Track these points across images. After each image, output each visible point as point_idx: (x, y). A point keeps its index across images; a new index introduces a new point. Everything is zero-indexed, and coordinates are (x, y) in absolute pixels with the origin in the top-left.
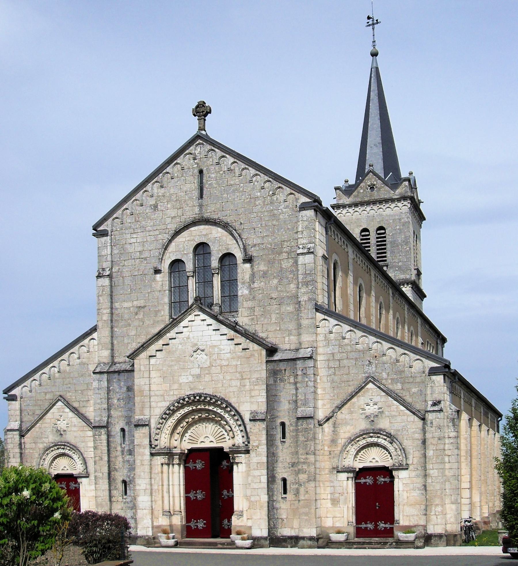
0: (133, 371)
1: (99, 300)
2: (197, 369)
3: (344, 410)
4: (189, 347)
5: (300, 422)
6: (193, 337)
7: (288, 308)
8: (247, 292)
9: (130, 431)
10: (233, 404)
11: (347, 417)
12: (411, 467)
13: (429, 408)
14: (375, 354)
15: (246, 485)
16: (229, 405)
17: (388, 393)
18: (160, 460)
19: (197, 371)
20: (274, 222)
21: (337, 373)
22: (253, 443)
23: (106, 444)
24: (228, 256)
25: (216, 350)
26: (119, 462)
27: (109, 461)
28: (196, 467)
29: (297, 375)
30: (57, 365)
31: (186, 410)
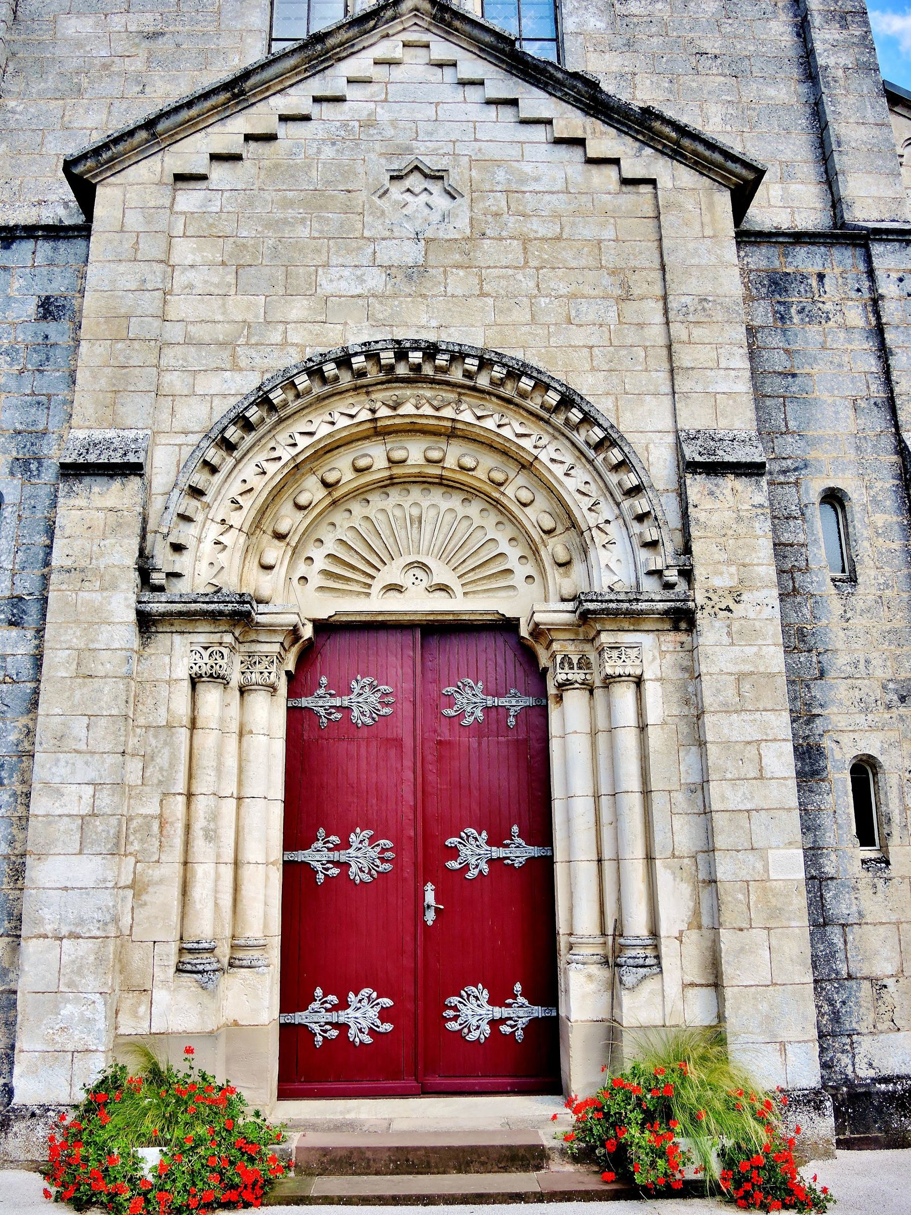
0: (84, 231)
2: (408, 246)
4: (373, 156)
6: (394, 123)
7: (771, 92)
8: (601, 25)
18: (180, 653)
19: (412, 253)
22: (713, 574)
25: (501, 175)
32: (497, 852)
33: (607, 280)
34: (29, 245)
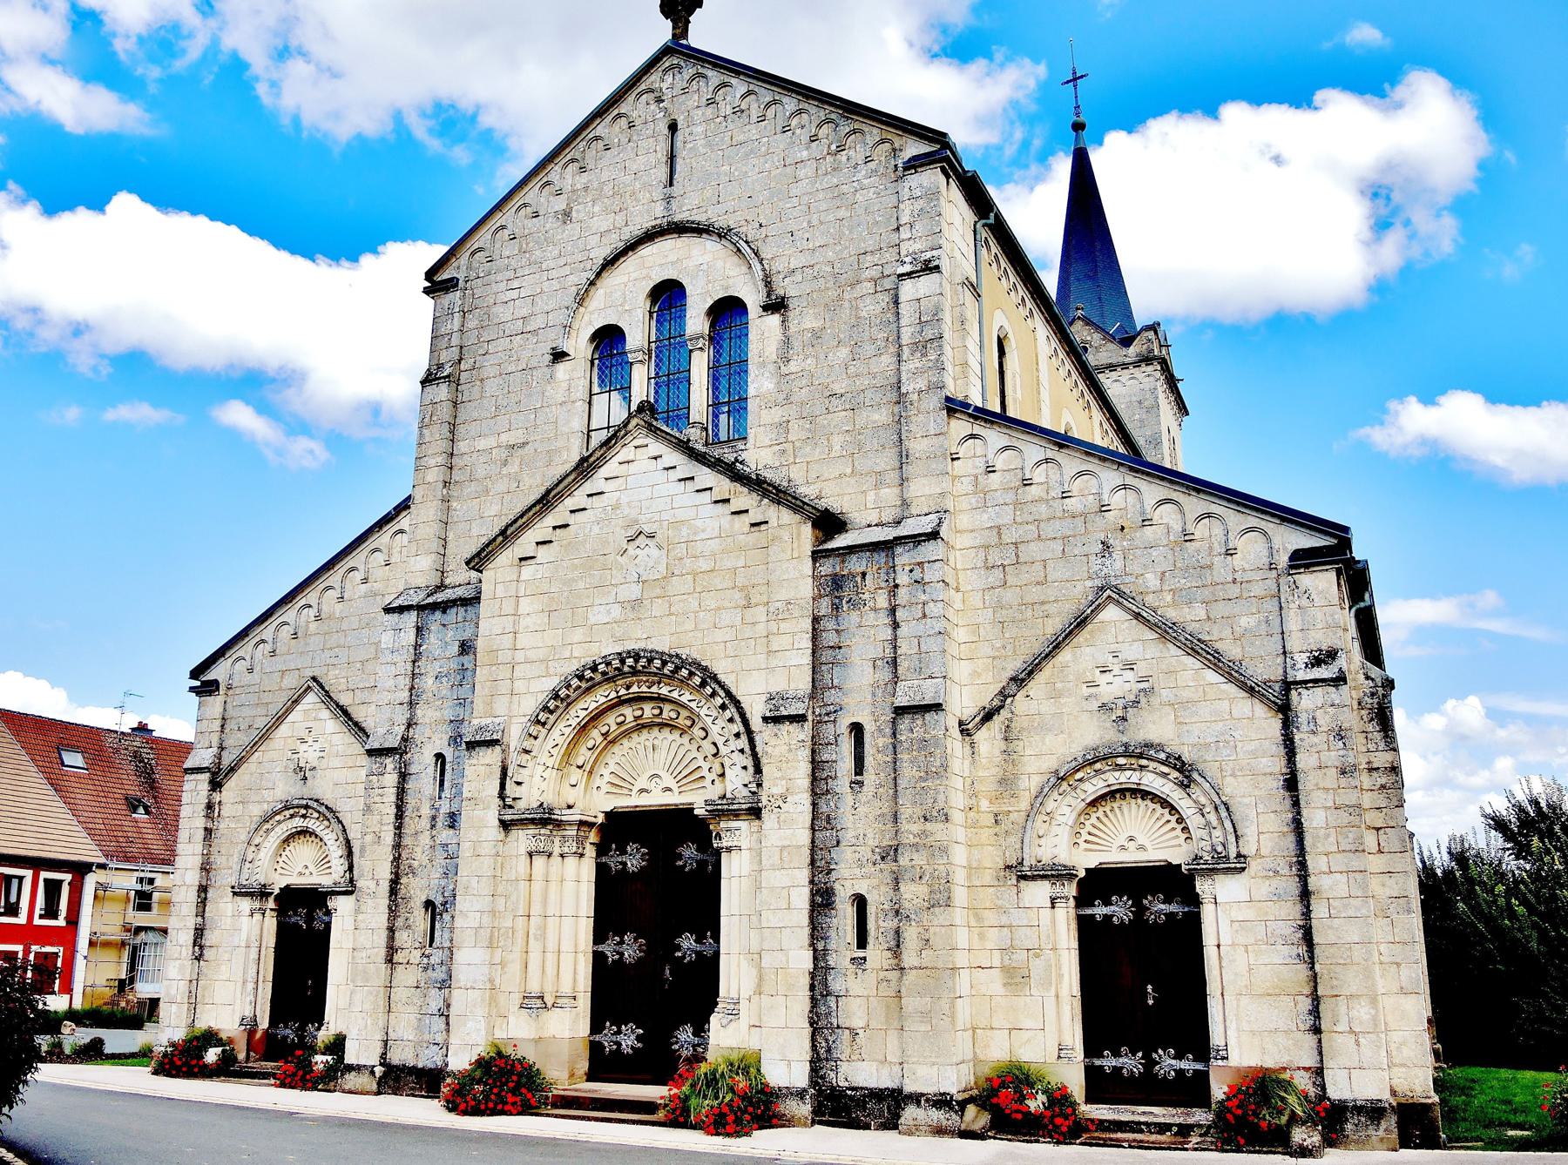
1: (421, 435)
3: (1036, 686)
5: (905, 723)
7: (876, 417)
8: (771, 386)
9: (457, 760)
10: (721, 677)
11: (1043, 709)
12: (1254, 866)
13: (1301, 676)
14: (1121, 522)
15: (754, 917)
16: (709, 677)
17: (1166, 631)
18: (523, 839)
19: (634, 591)
20: (842, 213)
21: (1011, 580)
22: (773, 784)
23: (393, 798)
24: (727, 311)
25: (685, 531)
26: (419, 849)
27: (397, 846)
28: (625, 864)
29: (896, 586)
30: (314, 603)
31: (600, 697)
32: (699, 948)
33: (737, 595)
34: (454, 610)
